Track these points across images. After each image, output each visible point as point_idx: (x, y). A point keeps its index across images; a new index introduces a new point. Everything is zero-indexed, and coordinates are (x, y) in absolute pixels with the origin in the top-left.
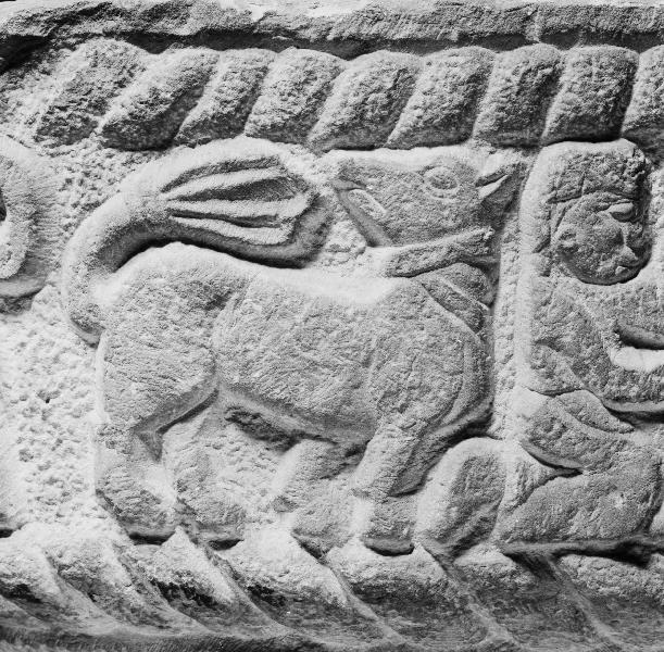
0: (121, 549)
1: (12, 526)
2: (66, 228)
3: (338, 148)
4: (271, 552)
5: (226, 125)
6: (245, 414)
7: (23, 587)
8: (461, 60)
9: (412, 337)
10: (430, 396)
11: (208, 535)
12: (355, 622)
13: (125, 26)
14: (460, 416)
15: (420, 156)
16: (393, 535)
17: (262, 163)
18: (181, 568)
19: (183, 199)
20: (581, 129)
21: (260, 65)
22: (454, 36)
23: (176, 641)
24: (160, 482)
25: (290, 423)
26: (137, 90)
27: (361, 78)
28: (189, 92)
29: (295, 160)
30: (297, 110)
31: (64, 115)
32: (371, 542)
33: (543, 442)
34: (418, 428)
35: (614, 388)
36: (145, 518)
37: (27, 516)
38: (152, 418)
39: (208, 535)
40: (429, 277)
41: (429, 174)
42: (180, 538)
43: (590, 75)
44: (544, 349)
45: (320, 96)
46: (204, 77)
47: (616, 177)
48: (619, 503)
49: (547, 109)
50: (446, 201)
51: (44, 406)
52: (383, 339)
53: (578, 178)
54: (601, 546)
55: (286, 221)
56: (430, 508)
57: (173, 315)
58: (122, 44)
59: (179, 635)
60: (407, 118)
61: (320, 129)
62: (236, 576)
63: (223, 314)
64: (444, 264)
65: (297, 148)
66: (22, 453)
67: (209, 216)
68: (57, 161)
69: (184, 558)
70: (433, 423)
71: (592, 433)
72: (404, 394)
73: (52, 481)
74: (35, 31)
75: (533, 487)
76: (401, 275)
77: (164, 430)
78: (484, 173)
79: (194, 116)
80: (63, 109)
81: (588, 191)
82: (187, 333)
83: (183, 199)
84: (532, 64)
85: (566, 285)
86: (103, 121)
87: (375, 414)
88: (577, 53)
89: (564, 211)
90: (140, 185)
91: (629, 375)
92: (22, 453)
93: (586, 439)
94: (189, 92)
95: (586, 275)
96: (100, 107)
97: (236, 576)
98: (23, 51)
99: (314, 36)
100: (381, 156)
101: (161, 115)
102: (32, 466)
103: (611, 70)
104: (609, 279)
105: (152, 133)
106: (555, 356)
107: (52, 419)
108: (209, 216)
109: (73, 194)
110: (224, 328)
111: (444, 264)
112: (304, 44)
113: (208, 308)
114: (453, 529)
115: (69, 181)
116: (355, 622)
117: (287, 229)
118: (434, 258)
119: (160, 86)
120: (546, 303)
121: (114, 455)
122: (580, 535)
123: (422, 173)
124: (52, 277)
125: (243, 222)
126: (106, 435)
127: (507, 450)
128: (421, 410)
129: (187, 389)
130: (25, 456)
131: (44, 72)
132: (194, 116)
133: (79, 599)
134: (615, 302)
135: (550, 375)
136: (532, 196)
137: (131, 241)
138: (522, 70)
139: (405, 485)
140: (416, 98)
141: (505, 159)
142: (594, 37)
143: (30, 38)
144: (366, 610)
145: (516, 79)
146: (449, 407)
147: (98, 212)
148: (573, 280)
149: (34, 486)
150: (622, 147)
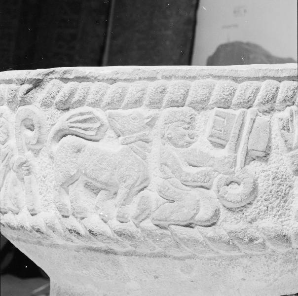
0: (60, 219)
1: (37, 212)
2: (48, 130)
3: (109, 109)
4: (94, 221)
5: (81, 103)
6: (89, 182)
7: (39, 229)
8: (139, 85)
9: (127, 161)
10: (132, 178)
11: (79, 216)
12: (117, 242)
13: (59, 76)
14: (140, 185)
15: (130, 111)
16: (123, 217)
17: (89, 113)
18: (72, 224)
19: (71, 123)
20: (174, 104)
21: (89, 86)
22: (137, 78)
23: (78, 246)
24: (66, 200)
25: (99, 185)
26: (61, 93)
27: (113, 90)
28: (72, 94)
29: (98, 112)
30: (97, 98)
31: (46, 100)
32: (119, 219)
33: (163, 192)
34: (129, 187)
35: (184, 178)
36: (63, 210)
37: (41, 210)
38: (65, 183)
39: (79, 216)
40: (132, 145)
41: (130, 116)
42: (71, 217)
43: (176, 89)
44: (163, 166)
45: (103, 95)
46: (258, 89)
47: (184, 118)
48: (186, 211)
50: (136, 124)
51: (44, 179)
52: (119, 162)
53: (173, 118)
54: (182, 224)
55: (95, 129)
56: (132, 209)
57: (69, 155)
58: (58, 81)
59: (78, 245)
60: (126, 101)
61: (103, 104)
62: (85, 227)
63: (80, 154)
64: (135, 141)
65: (98, 109)
66: (40, 192)
67: (77, 128)
68: (46, 113)
69: (73, 222)
70: (133, 186)
71: (177, 190)
72: (125, 177)
73: (46, 200)
74: (40, 77)
75: (160, 205)
76: (124, 144)
77: (68, 186)
78: (146, 116)
79: (74, 100)
80: (46, 99)
81: (175, 121)
82: (72, 159)
83: (71, 123)
84: (159, 85)
85: (170, 147)
86: (55, 102)
87: (118, 182)
88: (174, 81)
89: (169, 127)
90: (62, 120)
91: (188, 174)
92: (40, 192)
93: (175, 192)
94: (72, 94)
95: (175, 145)
96: (53, 98)
97: (85, 227)
98: (38, 83)
99: (102, 78)
100: (120, 111)
101: (67, 100)
102: (42, 196)
103: (182, 87)
104: (182, 147)
105: (64, 106)
106: (167, 168)
107: (46, 183)
108: (77, 128)
109: (49, 122)
111: (135, 141)
112: (99, 80)
113: (76, 152)
114: (139, 215)
115: (48, 118)
116: (117, 242)
117: (96, 131)
118: (133, 140)
119: (66, 92)
120: (163, 153)
122: (174, 220)
123: (129, 116)
124: (45, 144)
125: (85, 129)
127: (152, 194)
128: (130, 182)
129: (72, 174)
130: (41, 193)
131: (242, 90)
132: (74, 100)
133: (50, 232)
134: (184, 153)
135: (165, 174)
136: (159, 123)
137: (62, 134)
138: (156, 87)
139: (126, 201)
140: (128, 95)
141: (152, 112)
142: (176, 78)
143: (39, 79)
145: (154, 90)
146: (137, 181)
147: (54, 126)
148: (173, 147)
149: (42, 201)
150: (186, 109)
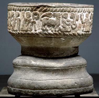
4: (50, 32)
5: (48, 11)
25: (51, 25)
49: (40, 67)
110: (48, 21)
121: (42, 27)
125: (49, 16)
126: (42, 26)
133: (40, 34)
144: (54, 35)
